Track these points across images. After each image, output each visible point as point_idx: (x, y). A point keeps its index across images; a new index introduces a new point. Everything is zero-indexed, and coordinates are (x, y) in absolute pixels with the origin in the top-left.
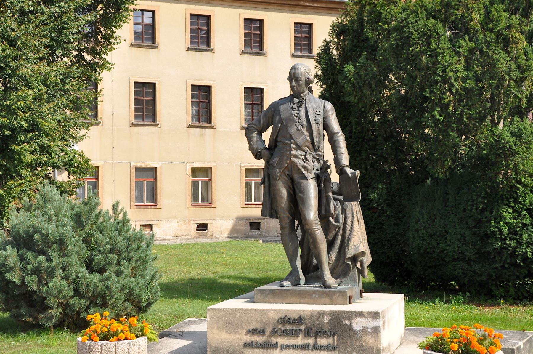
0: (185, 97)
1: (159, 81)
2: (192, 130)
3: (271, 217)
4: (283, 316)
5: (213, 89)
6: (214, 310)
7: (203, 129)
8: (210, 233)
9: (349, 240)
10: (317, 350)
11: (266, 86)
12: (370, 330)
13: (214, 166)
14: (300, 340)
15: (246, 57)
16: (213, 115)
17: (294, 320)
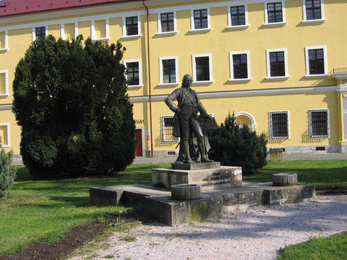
12: (239, 174)
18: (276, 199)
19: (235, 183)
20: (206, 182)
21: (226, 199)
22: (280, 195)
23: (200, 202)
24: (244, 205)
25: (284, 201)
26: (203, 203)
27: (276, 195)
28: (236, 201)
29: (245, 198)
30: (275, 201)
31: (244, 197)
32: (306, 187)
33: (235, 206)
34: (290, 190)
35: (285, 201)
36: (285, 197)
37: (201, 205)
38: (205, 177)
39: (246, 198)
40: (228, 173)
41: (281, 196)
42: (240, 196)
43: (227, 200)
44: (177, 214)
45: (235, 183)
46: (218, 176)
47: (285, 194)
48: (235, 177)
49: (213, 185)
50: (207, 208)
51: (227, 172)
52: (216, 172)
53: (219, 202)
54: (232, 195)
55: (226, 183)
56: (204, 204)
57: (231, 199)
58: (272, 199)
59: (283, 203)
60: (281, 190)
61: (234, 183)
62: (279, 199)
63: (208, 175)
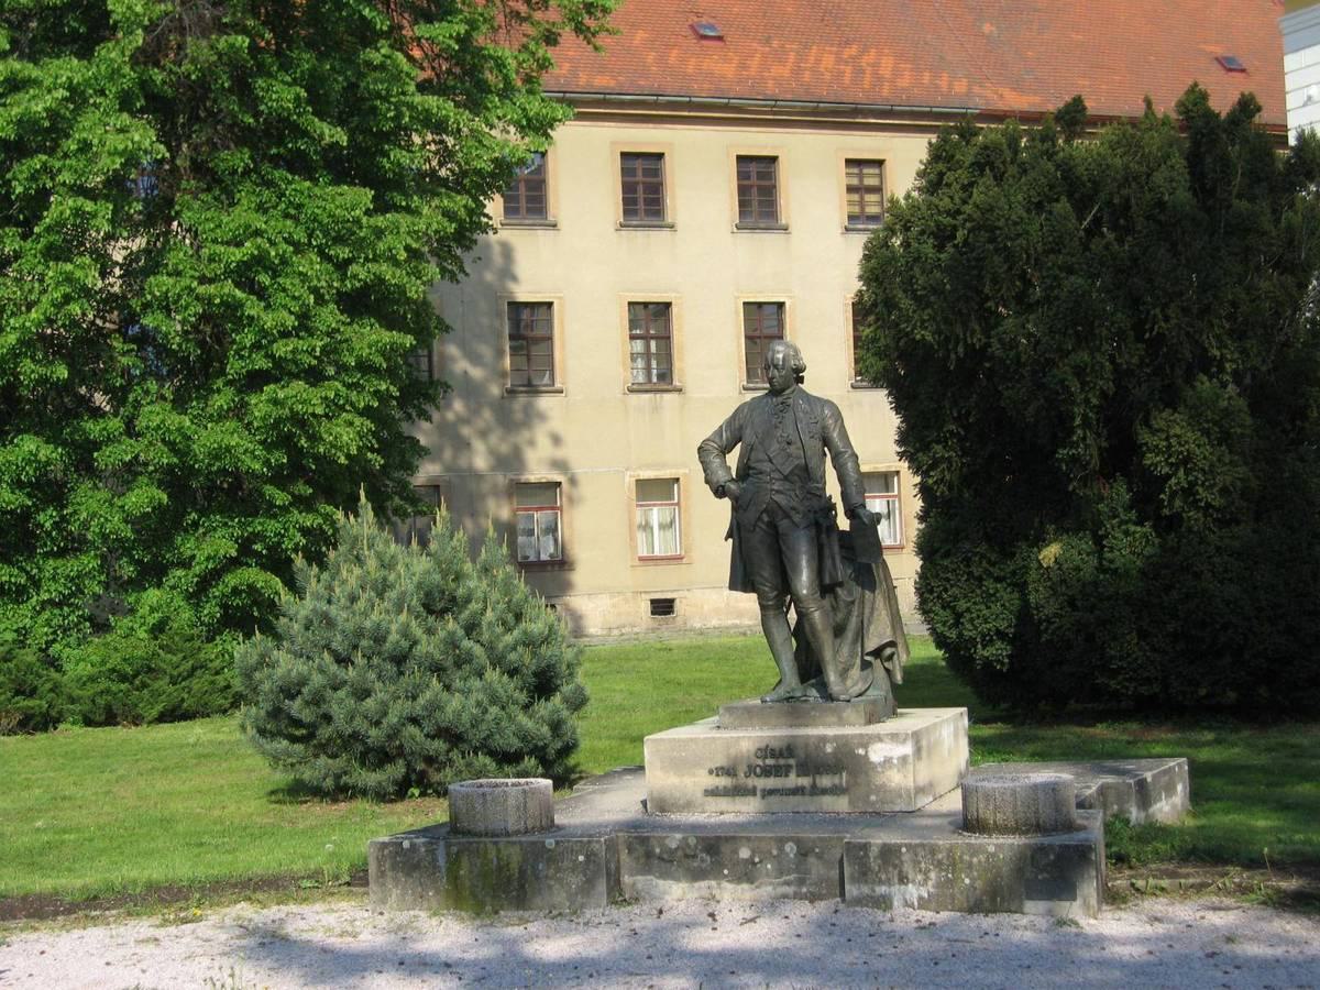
0: (617, 321)
1: (560, 298)
2: (634, 397)
3: (745, 590)
4: (763, 745)
5: (675, 310)
6: (656, 740)
7: (658, 396)
8: (679, 621)
9: (870, 623)
10: (816, 794)
11: (790, 297)
12: (895, 761)
13: (685, 474)
14: (793, 780)
15: (745, 236)
16: (677, 365)
17: (781, 750)
18: (874, 882)
19: (873, 798)
20: (723, 781)
21: (658, 850)
22: (895, 866)
23: (490, 846)
24: (745, 886)
25: (916, 896)
26: (504, 853)
27: (874, 864)
28: (704, 865)
29: (752, 857)
30: (866, 890)
31: (744, 853)
32: (1041, 850)
33: (703, 884)
34: (950, 850)
35: (920, 898)
36: (920, 877)
37: (492, 854)
38: (721, 761)
39: (757, 860)
40: (835, 753)
41: (900, 872)
42: (726, 849)
43: (665, 856)
44: (389, 874)
45: (873, 798)
46: (782, 762)
47: (923, 865)
48: (871, 773)
49: (758, 793)
50: (522, 872)
51: (829, 749)
52: (775, 745)
53: (581, 858)
54: (685, 839)
55: (824, 792)
56: (509, 856)
57: (680, 853)
58: (854, 880)
59: (907, 904)
60: (900, 846)
61: (868, 797)
62: (889, 882)
63: (733, 751)
